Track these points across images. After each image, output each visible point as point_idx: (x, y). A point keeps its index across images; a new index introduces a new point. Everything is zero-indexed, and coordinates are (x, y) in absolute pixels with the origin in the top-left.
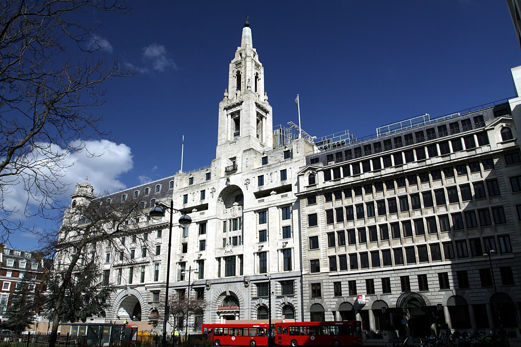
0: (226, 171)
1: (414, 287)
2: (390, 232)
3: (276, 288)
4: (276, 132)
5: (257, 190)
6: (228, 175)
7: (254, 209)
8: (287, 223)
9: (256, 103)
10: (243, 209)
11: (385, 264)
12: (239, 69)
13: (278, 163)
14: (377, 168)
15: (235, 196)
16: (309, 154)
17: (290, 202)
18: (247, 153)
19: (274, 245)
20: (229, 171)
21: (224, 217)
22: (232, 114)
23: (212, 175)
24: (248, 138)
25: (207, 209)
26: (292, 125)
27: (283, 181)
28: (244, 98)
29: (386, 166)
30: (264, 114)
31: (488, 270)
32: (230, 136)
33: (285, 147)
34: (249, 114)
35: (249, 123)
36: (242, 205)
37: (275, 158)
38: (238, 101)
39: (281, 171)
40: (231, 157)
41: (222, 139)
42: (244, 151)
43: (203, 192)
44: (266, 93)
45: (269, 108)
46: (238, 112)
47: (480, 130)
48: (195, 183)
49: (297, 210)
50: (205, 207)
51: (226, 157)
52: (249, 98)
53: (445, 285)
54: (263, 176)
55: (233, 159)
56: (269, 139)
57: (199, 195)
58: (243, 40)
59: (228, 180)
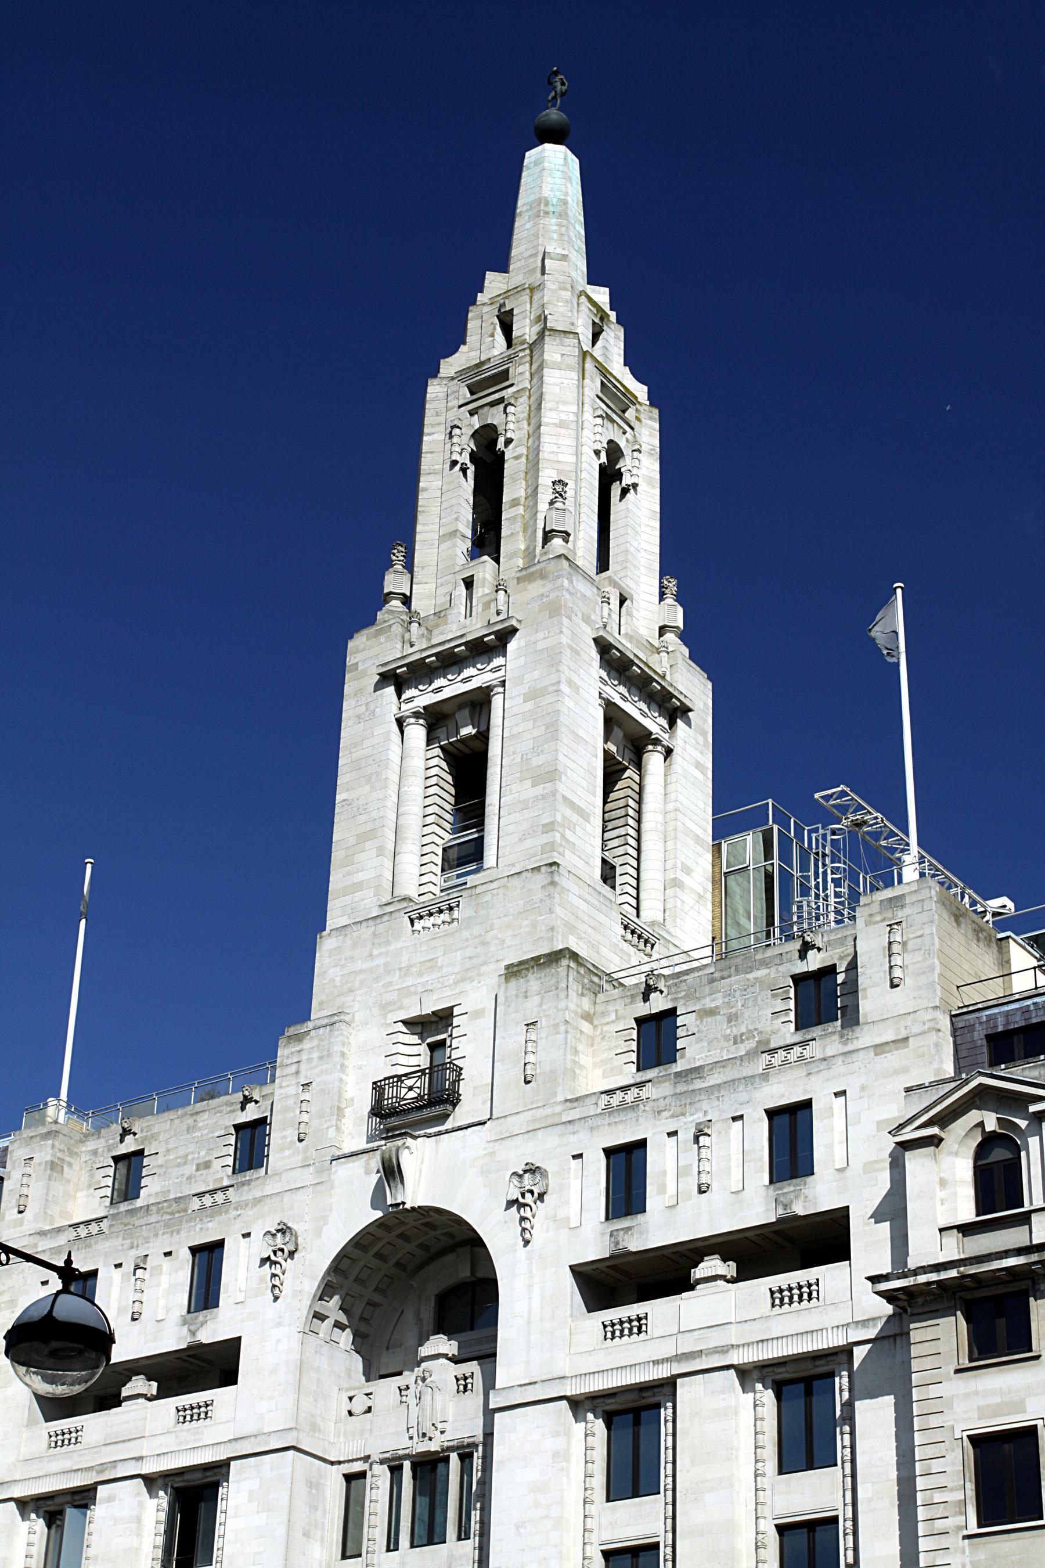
0: (377, 1111)
4: (736, 853)
5: (593, 1245)
6: (390, 1134)
7: (572, 1389)
8: (813, 1493)
9: (604, 647)
10: (489, 1383)
12: (495, 417)
13: (751, 1055)
15: (433, 1290)
16: (973, 996)
17: (836, 1340)
18: (533, 981)
20: (394, 1112)
21: (348, 1443)
22: (436, 719)
23: (279, 1137)
24: (541, 878)
25: (229, 1377)
26: (844, 809)
27: (788, 1187)
28: (521, 605)
30: (654, 723)
32: (417, 871)
33: (806, 948)
34: (549, 721)
35: (550, 775)
36: (488, 1357)
37: (732, 1018)
38: (476, 628)
39: (771, 1114)
40: (414, 1012)
41: (358, 887)
42: (514, 971)
43: (208, 1257)
44: (672, 585)
45: (694, 687)
46: (478, 703)
48: (151, 1189)
49: (1038, 1138)
50: (210, 1367)
51: (385, 1008)
52: (554, 610)
54: (642, 1144)
55: (433, 1026)
56: (689, 899)
57: (175, 1278)
58: (523, 226)
59: (392, 1172)
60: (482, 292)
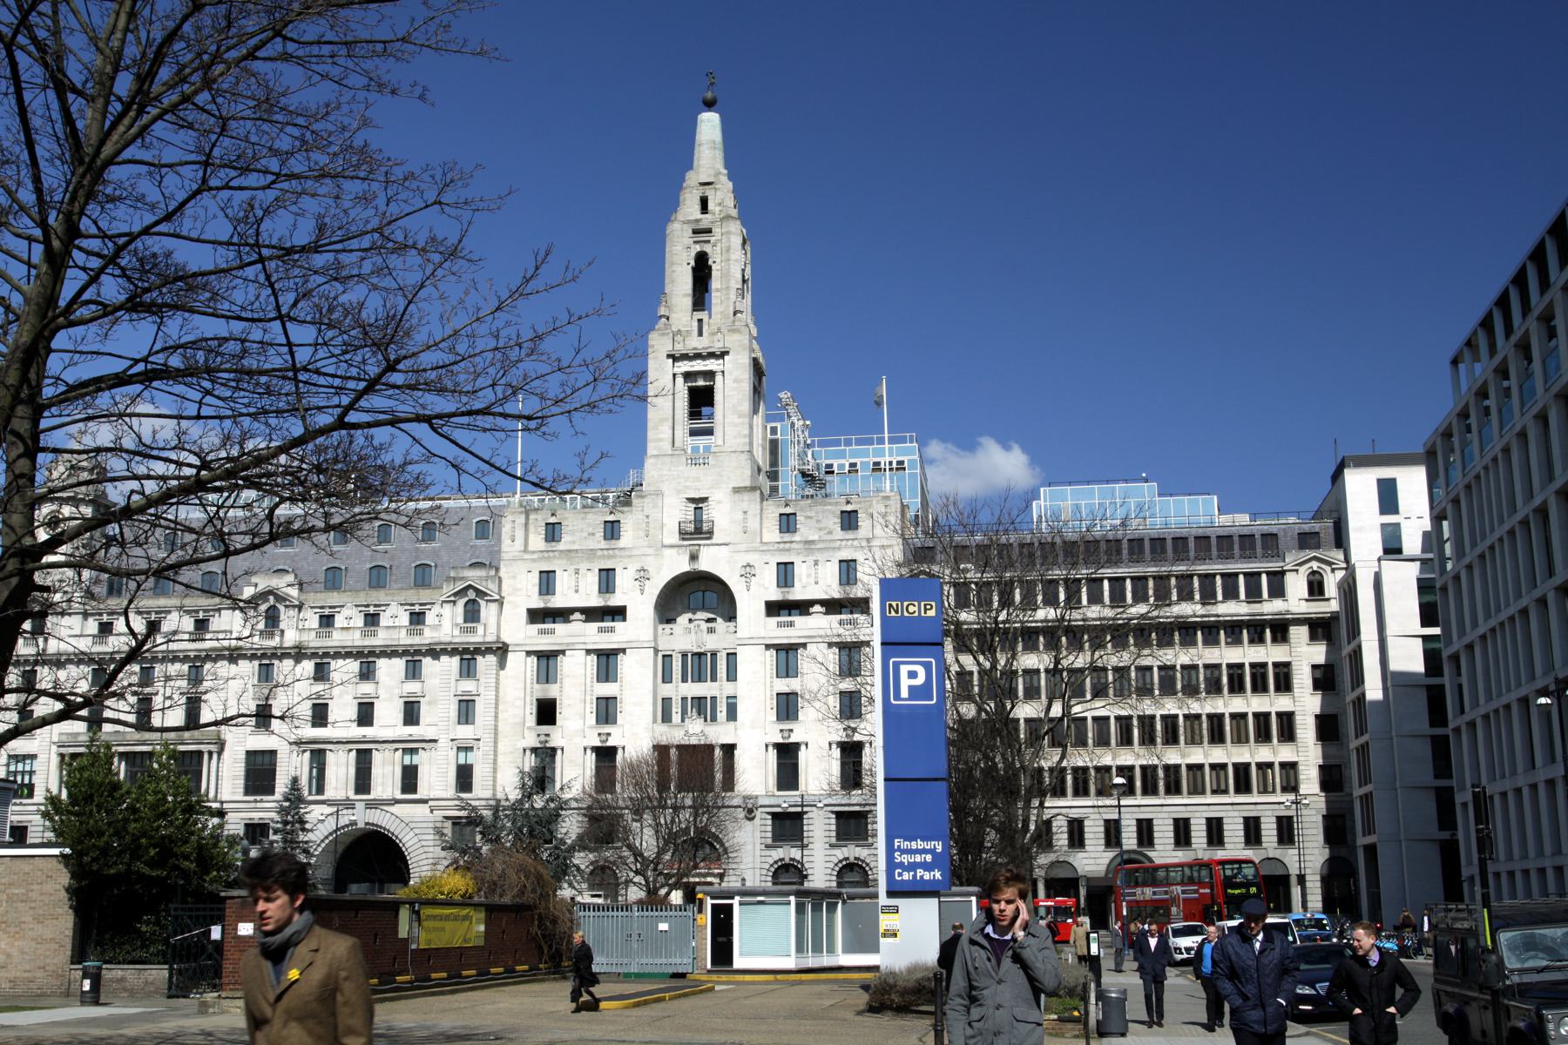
1: (1129, 840)
2: (1136, 732)
3: (819, 827)
11: (1145, 792)
14: (1118, 599)
19: (818, 735)
29: (1092, 601)
31: (1290, 818)
47: (1274, 566)
51: (679, 492)
53: (1113, 840)
57: (591, 581)
60: (1425, 534)
